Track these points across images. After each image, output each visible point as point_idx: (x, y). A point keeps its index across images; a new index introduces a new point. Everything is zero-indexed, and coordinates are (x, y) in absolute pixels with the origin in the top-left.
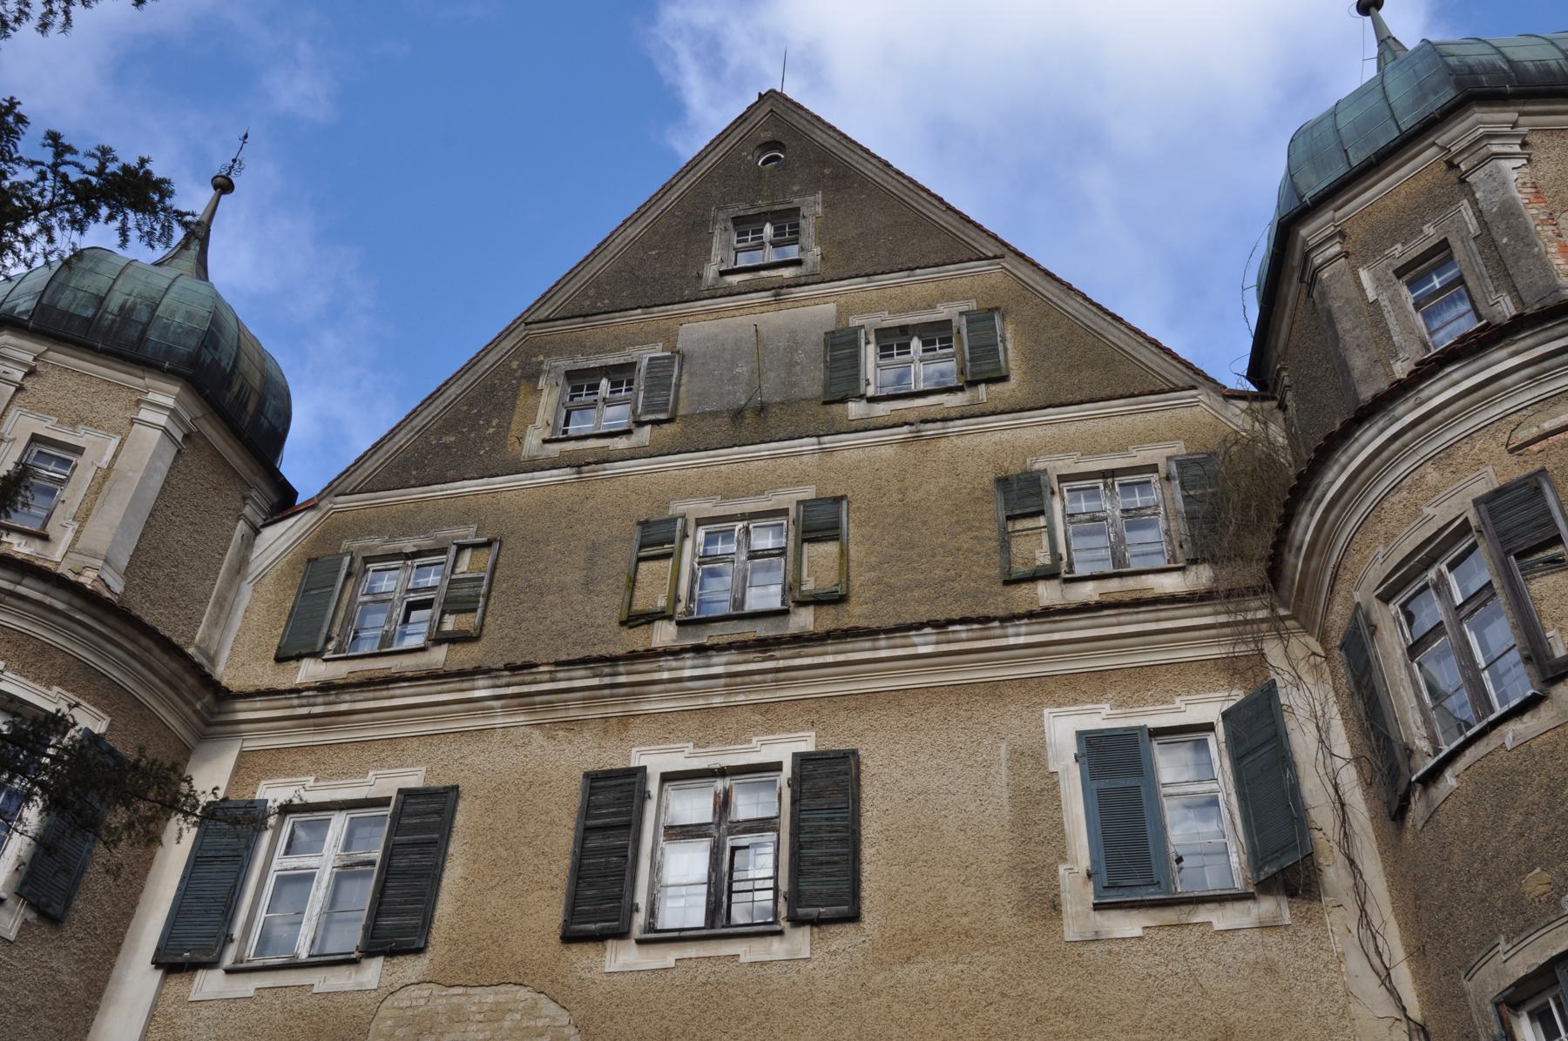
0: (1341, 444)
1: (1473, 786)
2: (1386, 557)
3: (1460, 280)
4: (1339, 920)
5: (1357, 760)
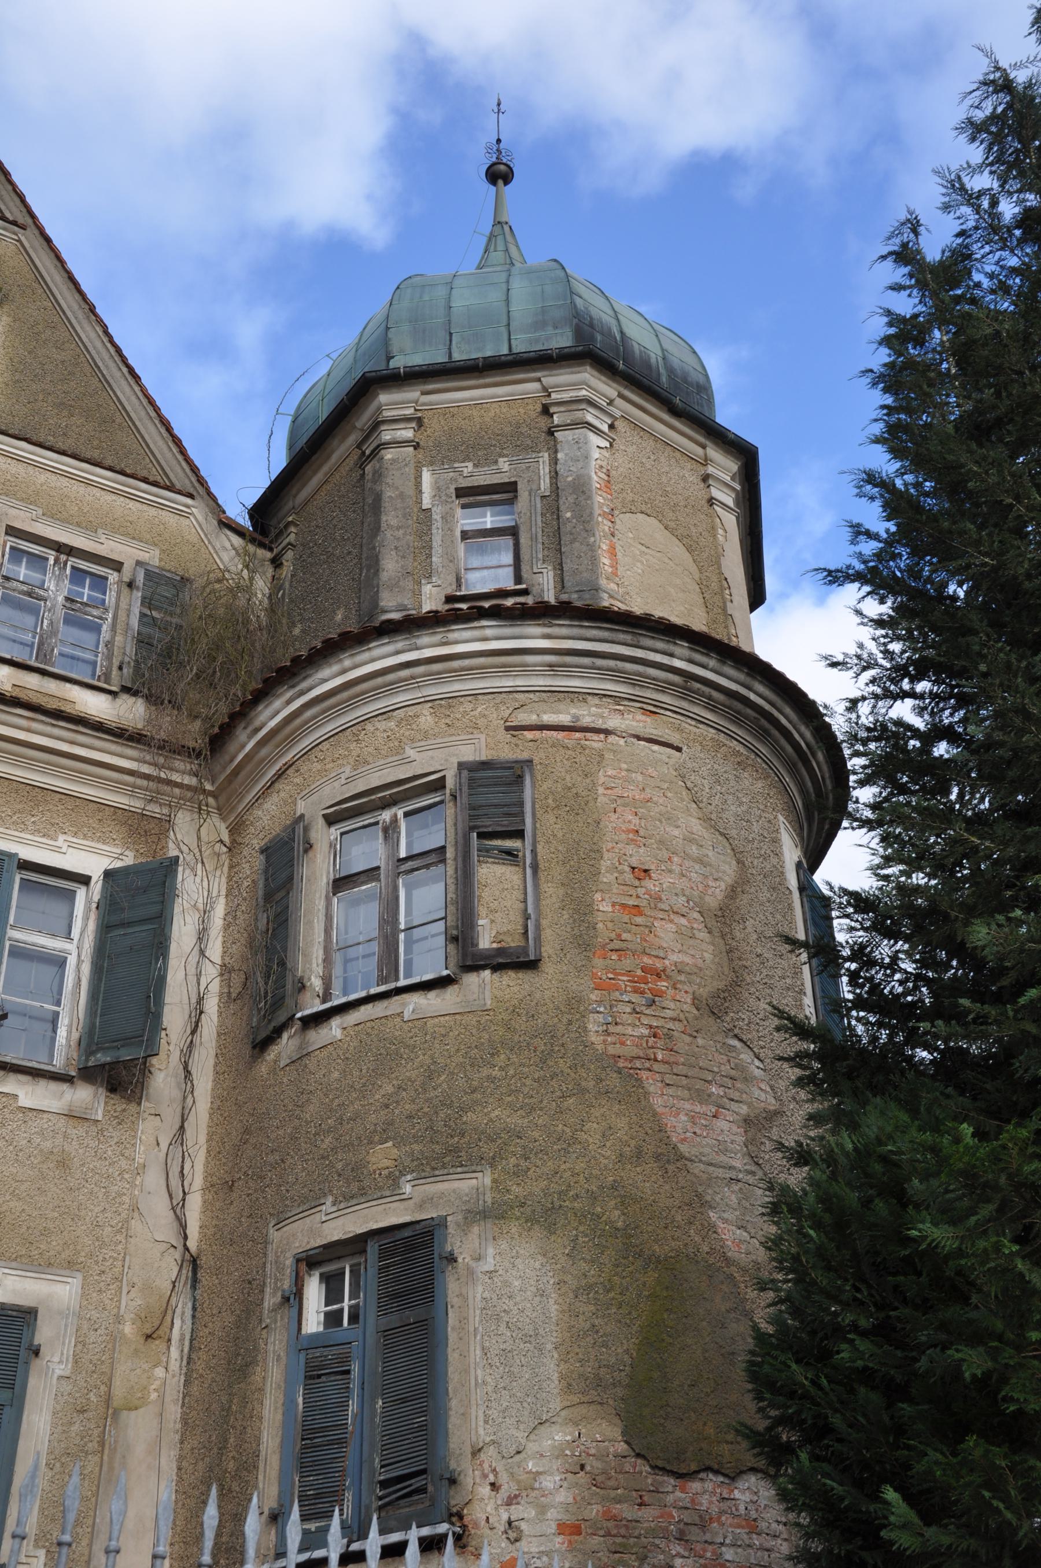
0: (351, 647)
1: (356, 1043)
2: (350, 780)
3: (513, 532)
4: (151, 1130)
5: (226, 970)
